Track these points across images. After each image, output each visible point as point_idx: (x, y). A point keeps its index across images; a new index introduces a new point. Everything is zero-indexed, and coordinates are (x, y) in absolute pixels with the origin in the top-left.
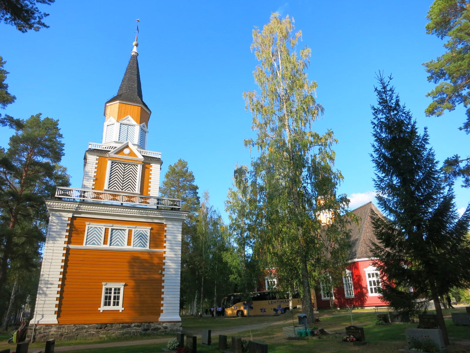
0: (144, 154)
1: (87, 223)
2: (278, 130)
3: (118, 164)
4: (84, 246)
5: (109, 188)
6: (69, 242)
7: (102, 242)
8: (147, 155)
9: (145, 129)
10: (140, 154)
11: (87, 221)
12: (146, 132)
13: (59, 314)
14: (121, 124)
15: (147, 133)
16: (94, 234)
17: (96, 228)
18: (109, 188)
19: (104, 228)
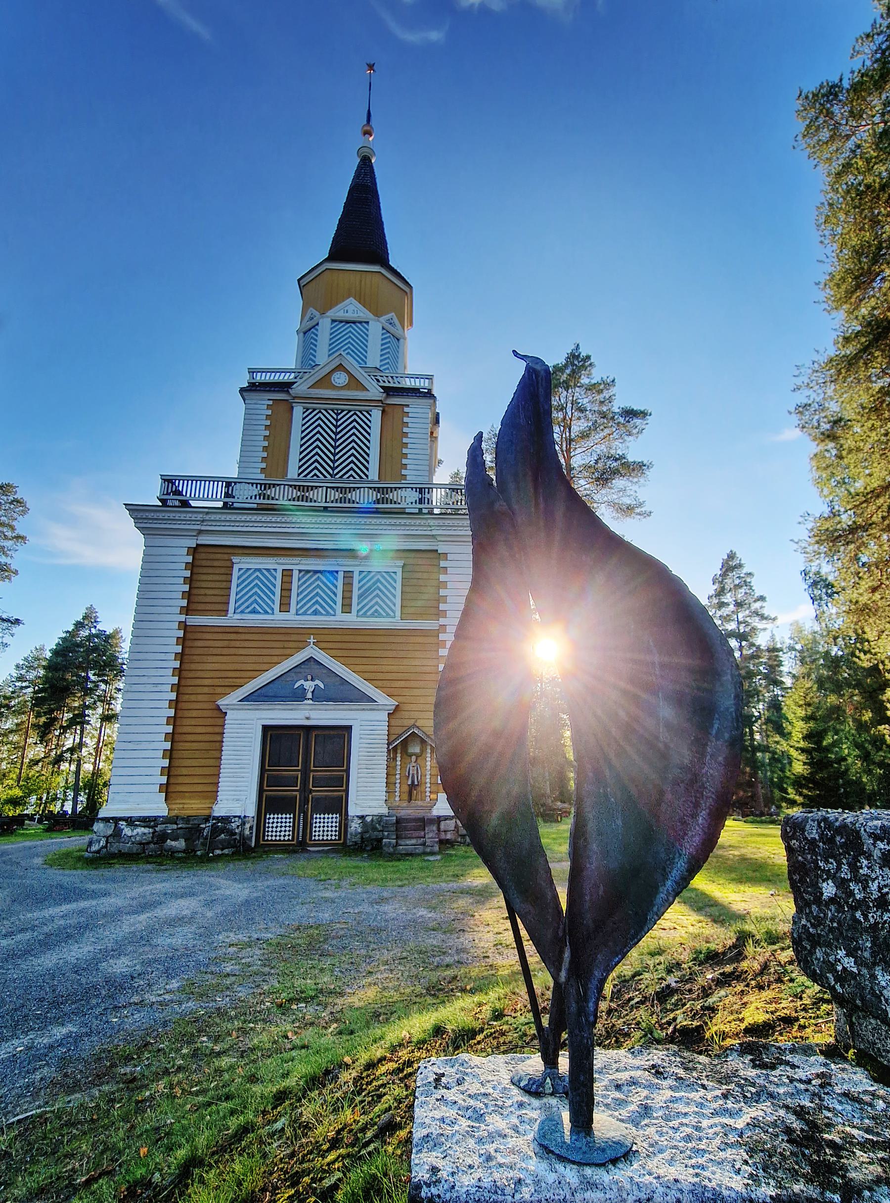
0: (387, 384)
1: (235, 559)
2: (491, 972)
3: (320, 412)
4: (233, 619)
5: (299, 475)
6: (186, 611)
7: (339, 607)
8: (392, 385)
9: (397, 331)
10: (375, 383)
11: (234, 554)
12: (398, 340)
13: (167, 790)
14: (333, 321)
15: (401, 340)
16: (253, 588)
17: (259, 570)
18: (299, 475)
19: (280, 568)
